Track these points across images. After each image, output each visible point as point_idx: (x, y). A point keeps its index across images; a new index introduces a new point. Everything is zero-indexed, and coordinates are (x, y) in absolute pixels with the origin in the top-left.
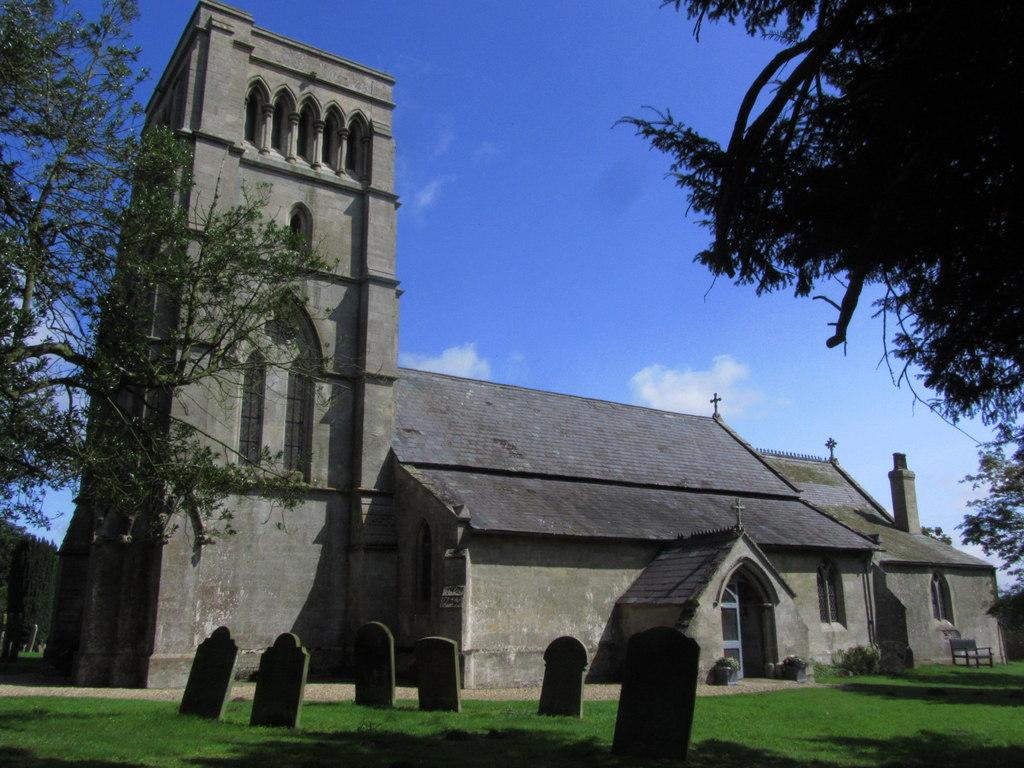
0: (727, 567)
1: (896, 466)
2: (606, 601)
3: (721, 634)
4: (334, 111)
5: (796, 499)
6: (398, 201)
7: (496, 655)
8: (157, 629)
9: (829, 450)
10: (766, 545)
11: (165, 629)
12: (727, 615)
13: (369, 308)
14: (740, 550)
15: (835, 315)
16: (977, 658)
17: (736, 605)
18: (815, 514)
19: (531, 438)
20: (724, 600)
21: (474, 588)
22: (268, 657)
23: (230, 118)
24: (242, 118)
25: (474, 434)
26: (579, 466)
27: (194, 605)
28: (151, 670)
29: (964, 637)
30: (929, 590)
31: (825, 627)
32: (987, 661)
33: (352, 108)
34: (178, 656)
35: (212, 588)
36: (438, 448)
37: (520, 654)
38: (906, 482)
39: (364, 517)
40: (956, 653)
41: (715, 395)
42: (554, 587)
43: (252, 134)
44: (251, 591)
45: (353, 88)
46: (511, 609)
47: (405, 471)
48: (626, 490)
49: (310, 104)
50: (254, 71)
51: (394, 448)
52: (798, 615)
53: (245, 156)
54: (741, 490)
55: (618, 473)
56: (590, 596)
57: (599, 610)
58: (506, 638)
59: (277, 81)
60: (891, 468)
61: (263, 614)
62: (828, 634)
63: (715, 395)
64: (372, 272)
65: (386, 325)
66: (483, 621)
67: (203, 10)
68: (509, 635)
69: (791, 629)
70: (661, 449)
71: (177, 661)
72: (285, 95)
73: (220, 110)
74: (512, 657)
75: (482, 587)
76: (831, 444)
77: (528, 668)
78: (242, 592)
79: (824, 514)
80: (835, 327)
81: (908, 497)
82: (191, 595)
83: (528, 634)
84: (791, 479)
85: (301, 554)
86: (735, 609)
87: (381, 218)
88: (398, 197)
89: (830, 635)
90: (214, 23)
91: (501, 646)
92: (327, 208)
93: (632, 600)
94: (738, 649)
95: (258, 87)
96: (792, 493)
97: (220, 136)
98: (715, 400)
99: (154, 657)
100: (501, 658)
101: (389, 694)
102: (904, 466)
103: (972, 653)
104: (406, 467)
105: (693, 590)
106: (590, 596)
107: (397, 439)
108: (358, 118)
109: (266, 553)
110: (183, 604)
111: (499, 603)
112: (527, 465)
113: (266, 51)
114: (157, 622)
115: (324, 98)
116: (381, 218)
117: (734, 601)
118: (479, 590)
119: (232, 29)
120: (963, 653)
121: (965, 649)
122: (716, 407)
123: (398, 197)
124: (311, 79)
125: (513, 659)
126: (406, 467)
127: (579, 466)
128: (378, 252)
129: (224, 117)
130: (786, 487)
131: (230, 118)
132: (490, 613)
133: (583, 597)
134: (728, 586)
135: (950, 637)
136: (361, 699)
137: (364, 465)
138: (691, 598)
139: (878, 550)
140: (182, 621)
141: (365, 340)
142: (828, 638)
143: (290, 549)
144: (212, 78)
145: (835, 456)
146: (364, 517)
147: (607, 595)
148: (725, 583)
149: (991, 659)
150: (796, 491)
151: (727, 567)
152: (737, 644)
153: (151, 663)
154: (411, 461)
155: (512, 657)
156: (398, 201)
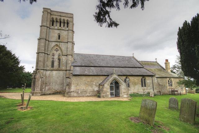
31: (143, 88)
58: (79, 90)
76: (156, 59)
106: (94, 83)
108: (68, 20)
117: (113, 84)
132: (76, 86)
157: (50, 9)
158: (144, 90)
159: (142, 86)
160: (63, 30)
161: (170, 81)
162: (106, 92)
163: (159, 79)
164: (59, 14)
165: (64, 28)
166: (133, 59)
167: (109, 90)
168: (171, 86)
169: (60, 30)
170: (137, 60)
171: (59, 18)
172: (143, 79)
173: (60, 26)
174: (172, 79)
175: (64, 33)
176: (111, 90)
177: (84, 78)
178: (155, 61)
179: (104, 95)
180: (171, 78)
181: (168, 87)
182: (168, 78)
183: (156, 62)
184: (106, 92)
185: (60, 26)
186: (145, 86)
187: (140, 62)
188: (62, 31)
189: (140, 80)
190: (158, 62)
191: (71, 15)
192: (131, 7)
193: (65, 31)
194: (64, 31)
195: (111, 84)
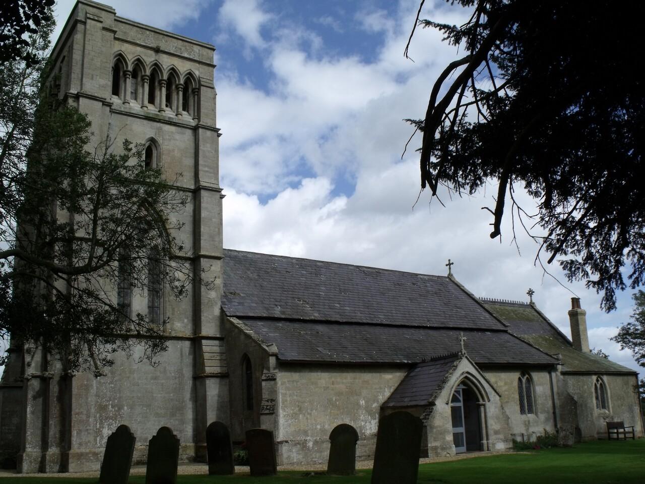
0: (454, 379)
1: (573, 307)
2: (374, 406)
3: (451, 423)
4: (173, 72)
5: (506, 332)
6: (219, 132)
7: (298, 443)
8: (73, 433)
9: (529, 297)
10: (479, 363)
11: (77, 433)
12: (455, 411)
13: (202, 209)
14: (465, 366)
15: (492, 219)
16: (625, 433)
17: (461, 404)
18: (517, 341)
19: (319, 296)
20: (452, 401)
21: (282, 400)
22: (154, 442)
23: (102, 82)
24: (108, 81)
25: (279, 295)
26: (353, 314)
27: (95, 417)
28: (70, 461)
29: (616, 420)
30: (593, 390)
31: (524, 417)
32: (631, 435)
33: (185, 69)
34: (88, 451)
35: (106, 405)
36: (254, 305)
37: (316, 442)
38: (579, 317)
39: (427, 182)
40: (611, 431)
41: (449, 260)
42: (338, 398)
43: (116, 91)
44: (132, 407)
45: (186, 55)
46: (308, 413)
47: (232, 323)
48: (408, 334)
49: (157, 67)
50: (118, 47)
51: (223, 306)
52: (503, 409)
53: (112, 108)
54: (467, 326)
55: (382, 319)
56: (362, 402)
57: (370, 413)
58: (305, 433)
59: (133, 54)
60: (570, 308)
61: (140, 422)
62: (525, 421)
63: (449, 260)
64: (203, 184)
65: (214, 220)
66: (290, 422)
67: (80, 5)
68: (307, 431)
69: (498, 418)
70: (410, 299)
71: (87, 454)
72: (139, 63)
73: (95, 77)
74: (310, 444)
75: (288, 399)
76: (531, 293)
77: (321, 452)
78: (126, 408)
79: (523, 341)
80: (493, 226)
81: (581, 327)
82: (93, 410)
83: (320, 429)
84: (502, 319)
85: (163, 381)
86: (460, 407)
87: (208, 145)
88: (220, 129)
89: (527, 423)
90: (88, 15)
91: (303, 438)
92: (170, 140)
93: (391, 404)
94: (462, 433)
95: (120, 59)
96: (502, 328)
97: (96, 95)
98: (449, 264)
99: (72, 451)
100: (303, 445)
101: (233, 469)
102: (579, 306)
103: (622, 430)
104: (232, 319)
105: (432, 395)
106: (362, 402)
107: (225, 300)
108: (190, 75)
109: (140, 382)
110: (88, 417)
111: (300, 410)
112: (316, 315)
113: (125, 33)
114: (72, 429)
115: (166, 62)
116: (208, 145)
117: (459, 401)
118: (286, 401)
119: (101, 20)
120: (616, 431)
121: (617, 428)
122: (450, 268)
123: (220, 129)
124: (157, 50)
125: (311, 446)
126: (232, 319)
127: (353, 314)
128: (206, 169)
129: (98, 82)
130: (499, 324)
131: (102, 82)
132: (294, 416)
133: (358, 404)
134: (455, 391)
135: (607, 420)
136: (211, 472)
137: (203, 318)
138: (431, 400)
139: (559, 364)
140: (88, 428)
141: (200, 232)
142: (525, 424)
143: (155, 378)
144: (89, 54)
145: (533, 301)
146: (427, 182)
147: (374, 401)
148: (453, 390)
149: (634, 434)
150: (504, 325)
151: (454, 379)
152: (462, 430)
153: (70, 456)
154: (234, 314)
155: (310, 444)
156: (219, 132)
157: (110, 11)
158: (527, 424)
159: (522, 411)
160: (170, 123)
161: (598, 386)
162: (443, 433)
163: (571, 380)
164: (152, 42)
165: (169, 113)
166: (451, 287)
167: (449, 425)
168: (604, 407)
169: (159, 125)
170: (470, 296)
171: (149, 58)
172: (524, 380)
173: (152, 100)
174: (605, 378)
175: (177, 137)
176: (455, 424)
177: (323, 378)
178: (526, 300)
179: (437, 444)
180: (603, 374)
181: (597, 412)
182: (595, 374)
183: (532, 306)
184: (443, 433)
185: (152, 100)
186: (530, 411)
187: (486, 306)
188: (167, 128)
189: (516, 383)
190: (539, 307)
191: (205, 52)
192: (640, 365)
193: (179, 129)
194: (173, 128)
195: (455, 399)
